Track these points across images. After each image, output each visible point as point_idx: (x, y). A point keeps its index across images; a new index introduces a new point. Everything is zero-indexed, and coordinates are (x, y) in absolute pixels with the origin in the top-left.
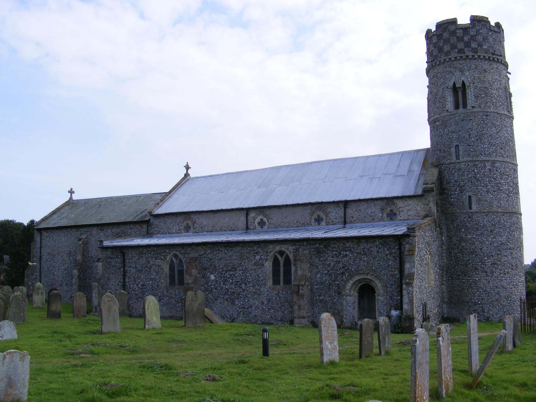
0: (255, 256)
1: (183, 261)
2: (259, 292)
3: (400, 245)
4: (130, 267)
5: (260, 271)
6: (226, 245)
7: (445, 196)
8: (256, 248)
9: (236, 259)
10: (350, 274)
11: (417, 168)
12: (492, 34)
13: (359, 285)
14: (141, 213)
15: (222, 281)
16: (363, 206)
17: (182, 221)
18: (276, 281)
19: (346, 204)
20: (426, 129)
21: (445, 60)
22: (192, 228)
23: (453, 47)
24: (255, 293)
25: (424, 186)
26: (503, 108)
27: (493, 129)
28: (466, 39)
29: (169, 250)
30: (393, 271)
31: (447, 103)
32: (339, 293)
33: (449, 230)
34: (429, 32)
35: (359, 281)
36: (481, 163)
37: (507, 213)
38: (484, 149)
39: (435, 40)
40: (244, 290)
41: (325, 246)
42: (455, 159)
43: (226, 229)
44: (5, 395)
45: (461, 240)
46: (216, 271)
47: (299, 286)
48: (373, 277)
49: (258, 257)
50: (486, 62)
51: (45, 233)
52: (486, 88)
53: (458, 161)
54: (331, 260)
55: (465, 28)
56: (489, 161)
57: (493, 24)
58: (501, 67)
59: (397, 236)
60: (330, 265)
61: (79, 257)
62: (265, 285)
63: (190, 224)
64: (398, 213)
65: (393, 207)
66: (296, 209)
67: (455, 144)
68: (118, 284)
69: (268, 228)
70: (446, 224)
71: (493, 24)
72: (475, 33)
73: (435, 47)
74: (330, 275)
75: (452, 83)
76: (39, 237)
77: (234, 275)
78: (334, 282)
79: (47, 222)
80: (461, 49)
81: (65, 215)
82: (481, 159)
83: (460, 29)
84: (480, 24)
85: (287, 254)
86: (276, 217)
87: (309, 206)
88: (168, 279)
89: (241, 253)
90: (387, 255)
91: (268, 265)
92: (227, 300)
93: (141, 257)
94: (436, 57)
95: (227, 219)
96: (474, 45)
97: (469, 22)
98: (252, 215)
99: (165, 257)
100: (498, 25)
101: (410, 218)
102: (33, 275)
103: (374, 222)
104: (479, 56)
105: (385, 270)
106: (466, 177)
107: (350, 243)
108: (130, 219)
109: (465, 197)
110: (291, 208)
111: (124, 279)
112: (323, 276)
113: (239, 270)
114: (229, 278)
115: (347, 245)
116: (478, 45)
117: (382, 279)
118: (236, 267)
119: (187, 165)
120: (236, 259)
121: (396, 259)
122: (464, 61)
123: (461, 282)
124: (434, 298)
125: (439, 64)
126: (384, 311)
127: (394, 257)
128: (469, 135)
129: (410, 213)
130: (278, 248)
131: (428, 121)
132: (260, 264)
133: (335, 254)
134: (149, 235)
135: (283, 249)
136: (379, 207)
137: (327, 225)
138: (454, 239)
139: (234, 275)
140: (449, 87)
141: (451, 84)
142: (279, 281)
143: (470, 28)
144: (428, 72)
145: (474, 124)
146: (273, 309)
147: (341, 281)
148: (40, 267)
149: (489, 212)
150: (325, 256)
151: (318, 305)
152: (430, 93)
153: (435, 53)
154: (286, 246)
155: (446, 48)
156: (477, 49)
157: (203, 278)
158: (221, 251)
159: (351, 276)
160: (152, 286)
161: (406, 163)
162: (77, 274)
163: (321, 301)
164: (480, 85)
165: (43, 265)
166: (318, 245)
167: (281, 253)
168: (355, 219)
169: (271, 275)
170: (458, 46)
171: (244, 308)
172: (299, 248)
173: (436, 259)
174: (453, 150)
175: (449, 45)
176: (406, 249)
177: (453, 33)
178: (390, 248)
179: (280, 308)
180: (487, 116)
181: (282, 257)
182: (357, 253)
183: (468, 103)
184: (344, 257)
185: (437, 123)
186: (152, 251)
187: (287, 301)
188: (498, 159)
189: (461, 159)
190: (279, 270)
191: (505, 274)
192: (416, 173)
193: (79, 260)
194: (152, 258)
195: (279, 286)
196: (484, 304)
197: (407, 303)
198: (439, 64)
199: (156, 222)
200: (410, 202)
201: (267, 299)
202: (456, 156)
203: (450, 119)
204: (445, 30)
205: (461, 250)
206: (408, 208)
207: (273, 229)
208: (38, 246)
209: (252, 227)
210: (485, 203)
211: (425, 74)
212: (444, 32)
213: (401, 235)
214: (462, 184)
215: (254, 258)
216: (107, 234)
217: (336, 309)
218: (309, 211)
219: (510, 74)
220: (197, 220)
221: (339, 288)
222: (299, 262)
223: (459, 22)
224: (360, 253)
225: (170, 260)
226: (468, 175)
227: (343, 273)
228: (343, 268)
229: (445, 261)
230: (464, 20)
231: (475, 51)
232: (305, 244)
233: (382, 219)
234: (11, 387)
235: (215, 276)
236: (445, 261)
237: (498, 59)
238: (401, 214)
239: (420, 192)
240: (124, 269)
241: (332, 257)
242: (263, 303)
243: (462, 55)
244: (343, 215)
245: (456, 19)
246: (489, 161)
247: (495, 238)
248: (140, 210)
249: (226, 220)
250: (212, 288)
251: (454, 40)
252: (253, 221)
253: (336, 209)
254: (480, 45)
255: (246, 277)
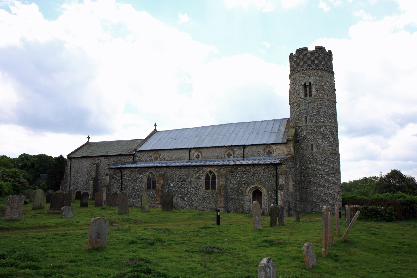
0: (196, 174)
1: (156, 176)
2: (198, 193)
3: (276, 169)
4: (125, 179)
5: (198, 182)
6: (180, 167)
7: (298, 144)
8: (196, 169)
9: (185, 175)
10: (248, 184)
11: (283, 129)
12: (327, 56)
13: (253, 190)
14: (130, 150)
15: (177, 187)
16: (254, 148)
17: (153, 154)
18: (207, 188)
19: (244, 146)
20: (288, 107)
21: (300, 70)
22: (159, 158)
23: (305, 63)
24: (196, 193)
25: (287, 138)
26: (331, 97)
27: (326, 108)
28: (312, 58)
29: (148, 170)
30: (272, 183)
31: (301, 93)
32: (242, 194)
33: (300, 162)
34: (291, 54)
35: (253, 188)
36: (319, 126)
37: (333, 154)
38: (321, 118)
39: (295, 59)
40: (189, 192)
41: (235, 169)
42: (304, 124)
43: (178, 159)
44: (96, 242)
45: (307, 167)
46: (174, 182)
47: (220, 190)
48: (261, 186)
49: (197, 174)
50: (323, 71)
51: (73, 160)
52: (322, 85)
53: (306, 125)
54: (238, 177)
55: (312, 53)
56: (323, 125)
57: (327, 51)
58: (331, 75)
59: (275, 164)
60: (237, 179)
61: (94, 174)
62: (201, 189)
63: (158, 156)
64: (273, 152)
65: (270, 149)
66: (217, 149)
67: (304, 116)
68: (118, 189)
69: (201, 159)
70: (299, 159)
71: (327, 51)
72: (317, 55)
73: (295, 63)
74: (238, 185)
75: (304, 83)
76: (70, 162)
77: (184, 184)
78: (240, 188)
79: (75, 154)
80: (310, 64)
81: (86, 150)
82: (319, 124)
83: (309, 53)
84: (320, 51)
85: (214, 173)
86: (206, 152)
87: (224, 148)
88: (147, 186)
89: (188, 172)
90: (269, 174)
91: (203, 178)
92: (180, 197)
93: (132, 173)
94: (295, 68)
95: (178, 154)
96: (317, 62)
97: (314, 50)
98: (193, 151)
99: (145, 174)
100: (330, 51)
101: (280, 155)
102: (65, 184)
103: (260, 157)
104: (319, 68)
105: (268, 182)
106: (310, 134)
107: (249, 167)
108: (124, 153)
109: (310, 144)
110: (214, 149)
111: (122, 186)
112: (233, 185)
113: (187, 181)
114: (182, 185)
115: (247, 168)
116: (319, 62)
117: (266, 187)
118: (185, 179)
119: (155, 124)
120: (185, 175)
121: (274, 177)
122: (311, 71)
123: (307, 190)
124: (293, 199)
125: (297, 72)
126: (267, 204)
127: (273, 175)
128: (313, 111)
129: (279, 152)
130: (209, 169)
131: (290, 103)
132: (199, 178)
133: (240, 173)
134: (134, 162)
135: (212, 170)
136: (262, 149)
137: (234, 158)
138: (303, 167)
139: (184, 184)
140: (302, 85)
141: (303, 83)
142: (209, 188)
143: (315, 53)
144: (290, 77)
145: (315, 105)
146: (205, 202)
147: (244, 188)
148: (70, 179)
149: (323, 153)
150: (234, 174)
151: (231, 201)
152: (291, 88)
153: (295, 66)
154: (213, 169)
155: (301, 63)
156: (318, 64)
157: (167, 185)
158: (177, 171)
159: (249, 185)
160: (138, 190)
161: (277, 126)
162: (92, 183)
163: (232, 198)
164: (319, 84)
165: (72, 178)
166: (231, 168)
167: (211, 172)
168: (249, 155)
169: (205, 185)
170: (308, 63)
171: (189, 202)
172: (221, 170)
173: (294, 178)
174: (303, 119)
175: (303, 62)
176: (280, 171)
177: (305, 55)
178: (270, 170)
179: (209, 202)
180: (322, 101)
181: (211, 174)
182: (253, 173)
183: (312, 94)
184: (245, 175)
185: (295, 104)
186: (138, 170)
187: (213, 199)
188: (328, 124)
189: (308, 124)
190: (209, 182)
191: (331, 186)
192: (282, 131)
193: (94, 175)
194: (138, 174)
195: (209, 190)
196: (320, 203)
197: (280, 200)
198: (297, 72)
199: (138, 155)
200: (280, 146)
201: (202, 197)
202: (305, 122)
203: (302, 102)
204: (301, 53)
205: (307, 173)
206: (278, 149)
207: (204, 160)
208: (69, 167)
209: (192, 159)
210: (321, 148)
211: (289, 78)
212: (300, 54)
213: (277, 164)
214: (308, 137)
215: (195, 175)
216: (110, 161)
217: (240, 203)
218: (224, 150)
219: (335, 78)
220: (161, 154)
221: (242, 192)
222: (221, 177)
223: (308, 50)
224: (254, 173)
225: (148, 175)
226: (311, 132)
227: (245, 184)
228: (244, 181)
229: (298, 179)
230: (311, 48)
231: (317, 65)
232: (224, 167)
233: (264, 155)
234: (99, 238)
235: (173, 184)
236: (298, 179)
237: (329, 70)
238: (275, 153)
239: (285, 141)
240: (122, 180)
241: (239, 175)
242: (200, 199)
243: (310, 67)
244: (243, 153)
245: (307, 47)
246: (323, 125)
247: (325, 167)
248: (129, 148)
249: (178, 154)
250: (171, 191)
251: (305, 59)
252: (193, 155)
253: (239, 150)
254: (320, 62)
255: (191, 185)
